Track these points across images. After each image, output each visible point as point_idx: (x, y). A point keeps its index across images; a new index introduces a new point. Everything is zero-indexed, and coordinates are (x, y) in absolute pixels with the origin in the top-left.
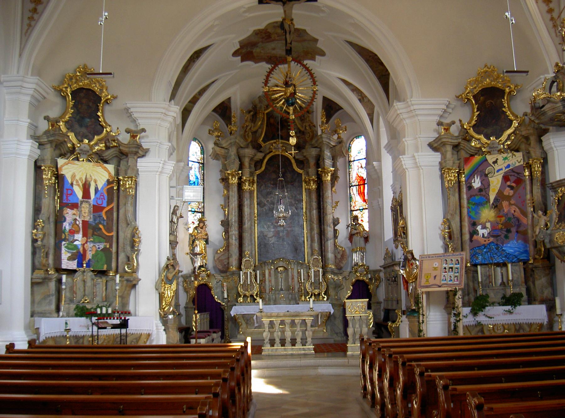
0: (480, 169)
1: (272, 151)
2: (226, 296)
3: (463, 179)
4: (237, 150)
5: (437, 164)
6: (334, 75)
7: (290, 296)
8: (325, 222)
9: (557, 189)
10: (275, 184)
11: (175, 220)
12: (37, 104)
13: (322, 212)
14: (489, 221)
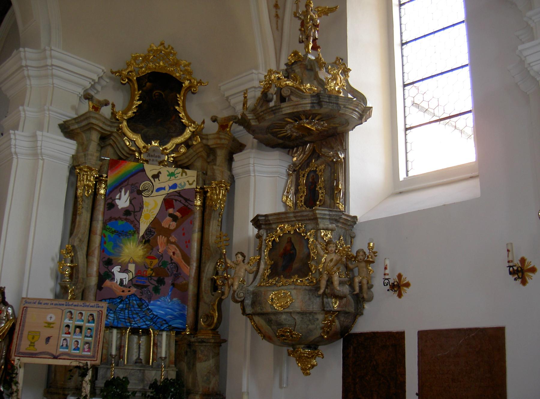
0: (132, 181)
3: (102, 191)
9: (274, 226)
14: (134, 262)
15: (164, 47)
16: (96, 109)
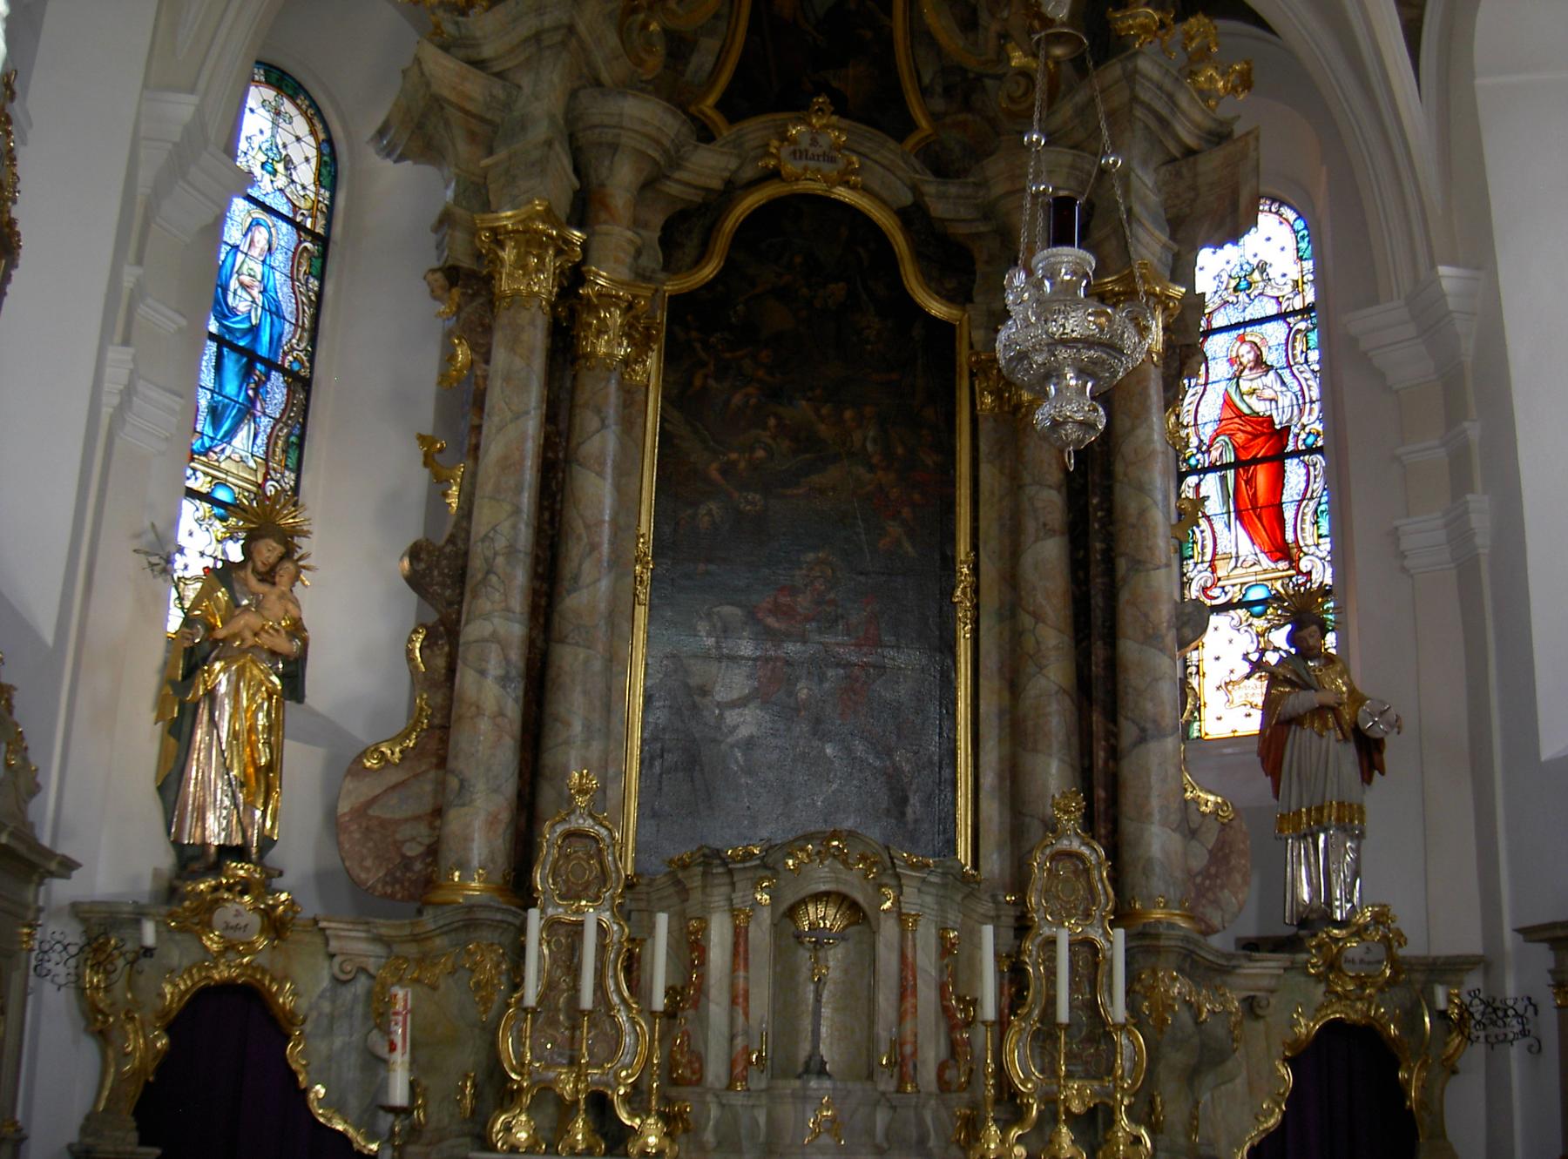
2: (399, 1094)
4: (573, 94)
7: (881, 1118)
8: (1127, 616)
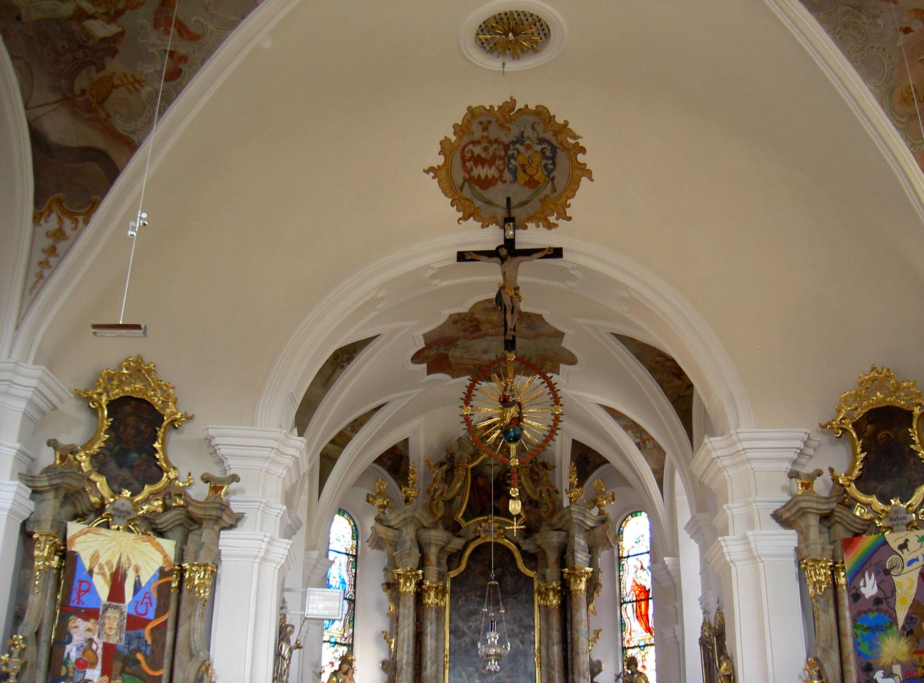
0: (874, 560)
1: (479, 537)
3: (842, 581)
4: (417, 530)
5: (791, 551)
6: (593, 400)
8: (575, 668)
10: (482, 596)
11: (285, 651)
12: (38, 418)
13: (569, 649)
14: (898, 662)
15: (877, 372)
16: (807, 486)
